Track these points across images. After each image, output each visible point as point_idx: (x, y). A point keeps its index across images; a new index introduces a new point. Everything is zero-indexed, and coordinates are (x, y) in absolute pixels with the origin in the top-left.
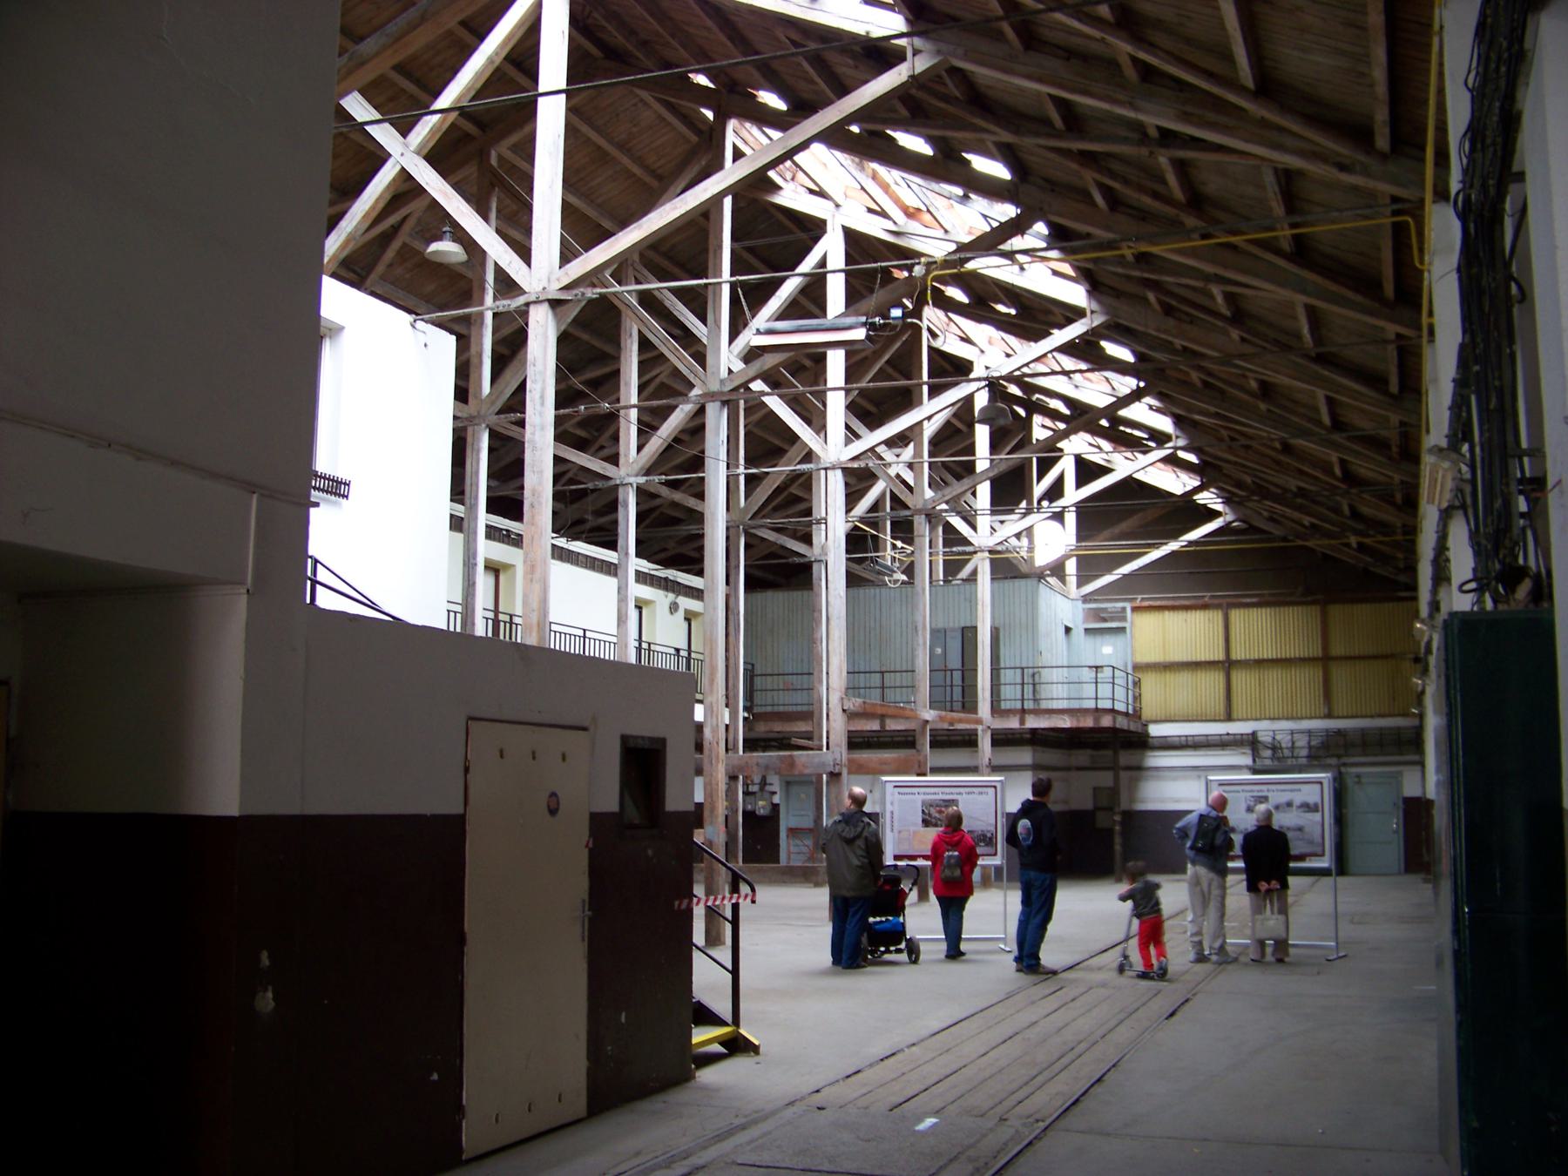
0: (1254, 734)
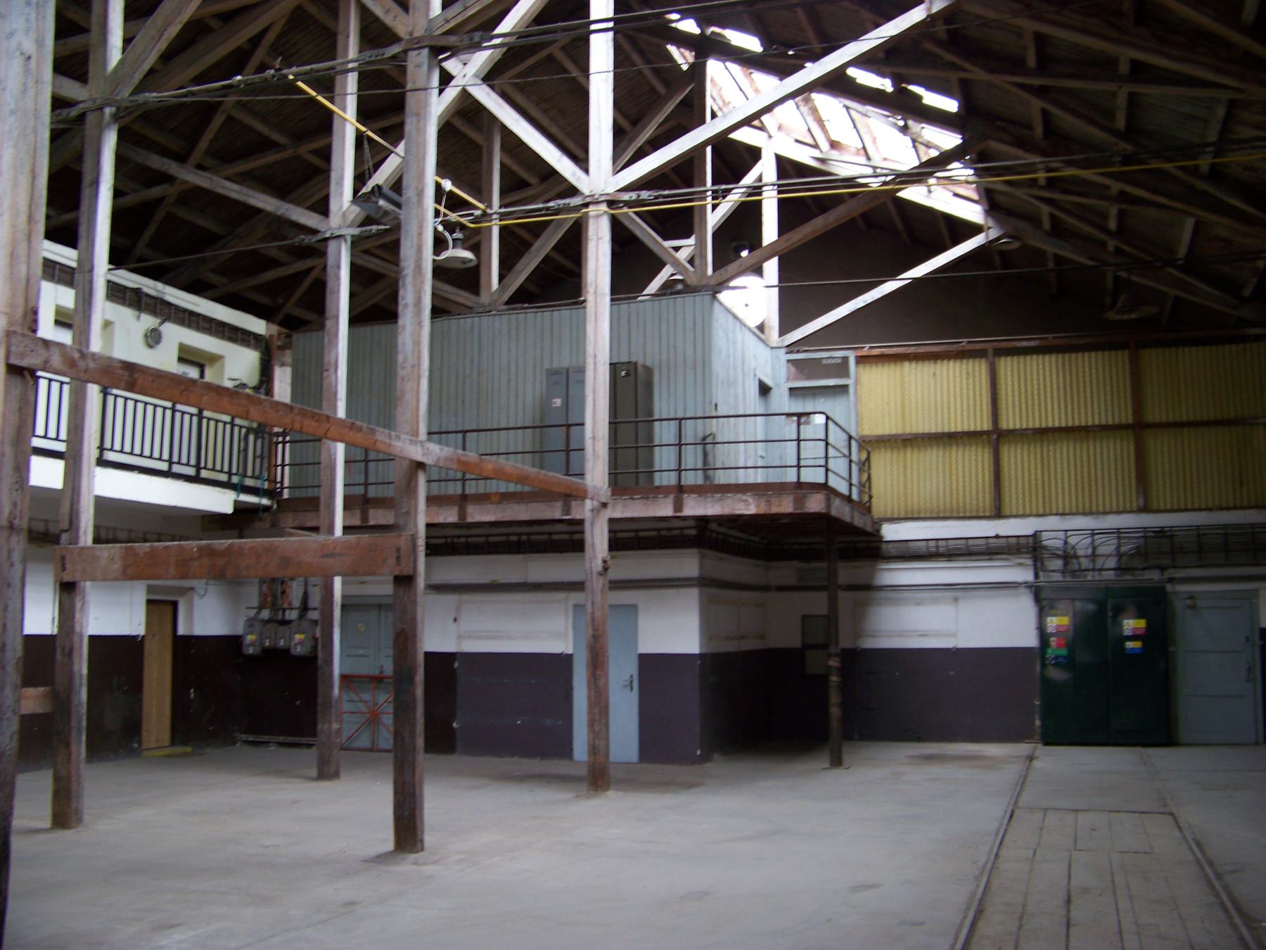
0: (1036, 535)
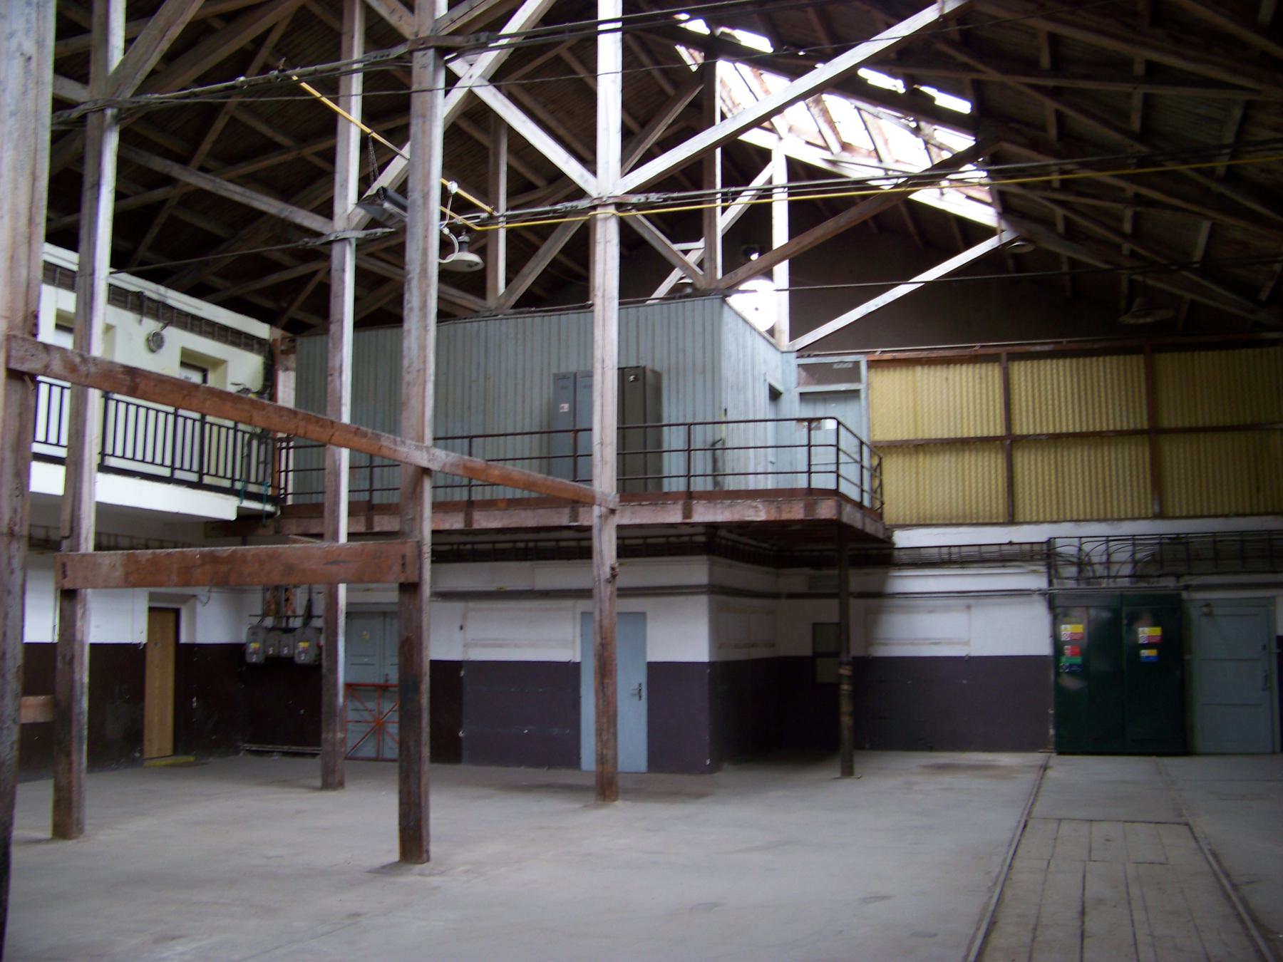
0: (1050, 542)
